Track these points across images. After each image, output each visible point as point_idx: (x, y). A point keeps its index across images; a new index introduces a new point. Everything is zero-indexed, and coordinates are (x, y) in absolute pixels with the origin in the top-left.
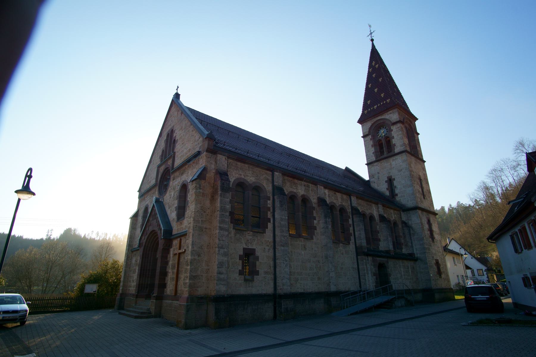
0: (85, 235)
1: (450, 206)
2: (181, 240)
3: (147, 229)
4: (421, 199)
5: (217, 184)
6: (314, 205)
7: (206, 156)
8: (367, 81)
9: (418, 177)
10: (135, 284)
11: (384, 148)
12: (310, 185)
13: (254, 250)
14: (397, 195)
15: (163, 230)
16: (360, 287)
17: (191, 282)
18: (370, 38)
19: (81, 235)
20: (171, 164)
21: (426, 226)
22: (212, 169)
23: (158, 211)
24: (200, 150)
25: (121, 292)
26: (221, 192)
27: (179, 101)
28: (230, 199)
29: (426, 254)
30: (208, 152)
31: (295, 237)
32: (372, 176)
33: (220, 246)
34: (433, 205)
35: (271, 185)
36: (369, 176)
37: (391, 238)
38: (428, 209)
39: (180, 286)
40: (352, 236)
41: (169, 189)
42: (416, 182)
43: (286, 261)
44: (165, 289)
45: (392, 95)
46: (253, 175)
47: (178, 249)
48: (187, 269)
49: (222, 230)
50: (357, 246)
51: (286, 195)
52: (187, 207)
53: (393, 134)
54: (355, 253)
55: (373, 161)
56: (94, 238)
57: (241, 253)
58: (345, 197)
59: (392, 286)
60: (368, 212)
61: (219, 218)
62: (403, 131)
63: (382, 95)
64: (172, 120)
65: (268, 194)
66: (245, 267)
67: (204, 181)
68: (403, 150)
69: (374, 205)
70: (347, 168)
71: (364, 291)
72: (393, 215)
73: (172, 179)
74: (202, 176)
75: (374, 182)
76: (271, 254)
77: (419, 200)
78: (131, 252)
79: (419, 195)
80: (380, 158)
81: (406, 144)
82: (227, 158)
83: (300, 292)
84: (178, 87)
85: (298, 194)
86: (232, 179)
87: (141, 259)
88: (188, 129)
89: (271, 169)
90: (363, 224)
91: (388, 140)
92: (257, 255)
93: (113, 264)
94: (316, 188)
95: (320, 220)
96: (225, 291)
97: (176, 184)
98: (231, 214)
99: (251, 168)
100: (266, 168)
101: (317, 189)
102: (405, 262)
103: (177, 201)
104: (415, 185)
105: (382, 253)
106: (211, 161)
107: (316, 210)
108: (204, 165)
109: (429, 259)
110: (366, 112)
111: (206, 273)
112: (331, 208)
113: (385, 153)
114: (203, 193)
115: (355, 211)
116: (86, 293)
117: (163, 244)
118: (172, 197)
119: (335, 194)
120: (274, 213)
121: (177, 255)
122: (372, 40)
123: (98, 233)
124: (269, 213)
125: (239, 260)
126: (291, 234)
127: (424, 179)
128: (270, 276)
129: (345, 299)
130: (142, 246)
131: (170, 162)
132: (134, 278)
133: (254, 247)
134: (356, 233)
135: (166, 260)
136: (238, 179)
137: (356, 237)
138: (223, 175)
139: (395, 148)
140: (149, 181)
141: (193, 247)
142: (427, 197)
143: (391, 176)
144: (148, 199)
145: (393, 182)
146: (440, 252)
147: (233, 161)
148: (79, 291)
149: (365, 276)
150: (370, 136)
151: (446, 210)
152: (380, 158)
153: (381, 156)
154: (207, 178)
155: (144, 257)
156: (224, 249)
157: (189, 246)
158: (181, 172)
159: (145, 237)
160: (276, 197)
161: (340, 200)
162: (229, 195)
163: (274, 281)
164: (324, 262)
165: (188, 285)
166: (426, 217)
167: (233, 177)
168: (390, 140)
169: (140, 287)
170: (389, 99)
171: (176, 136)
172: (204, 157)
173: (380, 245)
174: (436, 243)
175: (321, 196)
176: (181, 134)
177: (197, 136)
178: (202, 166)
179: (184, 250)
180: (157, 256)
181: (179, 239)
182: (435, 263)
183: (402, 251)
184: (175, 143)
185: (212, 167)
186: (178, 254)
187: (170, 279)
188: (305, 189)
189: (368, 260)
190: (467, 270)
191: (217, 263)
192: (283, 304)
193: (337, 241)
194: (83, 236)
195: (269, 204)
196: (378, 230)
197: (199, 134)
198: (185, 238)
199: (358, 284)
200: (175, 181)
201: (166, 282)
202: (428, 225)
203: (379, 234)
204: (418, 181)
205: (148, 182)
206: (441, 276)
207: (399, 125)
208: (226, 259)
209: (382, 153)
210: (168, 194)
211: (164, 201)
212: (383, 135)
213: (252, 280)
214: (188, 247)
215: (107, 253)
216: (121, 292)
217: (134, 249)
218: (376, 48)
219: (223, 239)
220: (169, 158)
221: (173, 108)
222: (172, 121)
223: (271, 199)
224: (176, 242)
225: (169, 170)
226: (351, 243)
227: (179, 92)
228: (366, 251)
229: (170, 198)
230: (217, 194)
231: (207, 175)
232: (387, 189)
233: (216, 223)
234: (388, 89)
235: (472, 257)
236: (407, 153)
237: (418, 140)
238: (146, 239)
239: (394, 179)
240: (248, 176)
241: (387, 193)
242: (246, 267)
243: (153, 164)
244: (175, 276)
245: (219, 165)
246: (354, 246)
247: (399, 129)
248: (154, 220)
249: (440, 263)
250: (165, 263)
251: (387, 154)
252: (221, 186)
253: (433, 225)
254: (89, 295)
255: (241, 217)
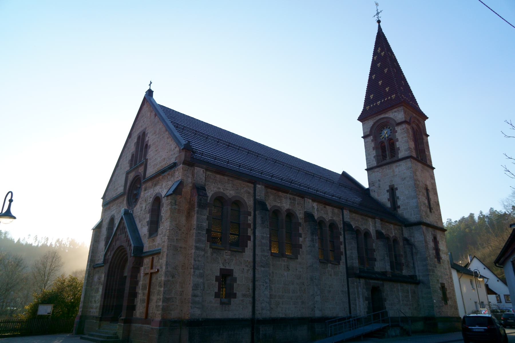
0: (19, 240)
1: (481, 213)
2: (153, 258)
3: (114, 244)
4: (426, 213)
5: (194, 200)
6: (300, 221)
7: (182, 169)
8: (371, 64)
9: (425, 187)
10: (98, 305)
11: (387, 152)
12: (297, 198)
13: (232, 271)
14: (399, 207)
15: (134, 246)
16: (465, 312)
17: (164, 304)
18: (376, 18)
19: (14, 239)
20: (143, 172)
21: (431, 245)
22: (189, 183)
23: (127, 225)
24: (176, 161)
25: (79, 313)
26: (198, 209)
27: (152, 100)
28: (207, 216)
29: (429, 276)
30: (185, 165)
31: (277, 257)
32: (372, 184)
33: (195, 266)
34: (442, 220)
35: (252, 199)
36: (369, 183)
37: (389, 258)
38: (435, 224)
39: (151, 308)
40: (343, 255)
41: (140, 200)
42: (421, 193)
43: (266, 283)
44: (134, 312)
45: (398, 90)
46: (233, 189)
47: (150, 269)
48: (160, 291)
49: (198, 250)
50: (348, 266)
51: (268, 211)
52: (161, 222)
53: (397, 136)
54: (345, 274)
55: (374, 166)
56: (31, 243)
57: (218, 274)
58: (336, 210)
59: (387, 312)
60: (363, 228)
61: (195, 236)
62: (409, 132)
63: (387, 89)
64: (144, 121)
65: (249, 209)
66: (221, 290)
67: (180, 196)
68: (408, 155)
69: (370, 220)
70: (344, 174)
71: (354, 317)
72: (392, 231)
73: (143, 189)
74: (178, 191)
75: (374, 191)
76: (250, 275)
77: (424, 214)
78: (93, 268)
79: (424, 208)
80: (382, 163)
81: (412, 148)
82: (205, 170)
83: (281, 317)
84: (151, 83)
85: (282, 208)
86: (210, 194)
87: (106, 278)
88: (162, 135)
89: (253, 180)
90: (356, 242)
91: (392, 142)
92: (235, 276)
93: (69, 281)
94: (303, 201)
95: (306, 238)
96: (199, 314)
97: (147, 196)
98: (208, 231)
99: (231, 181)
100: (248, 180)
101: (304, 202)
102: (405, 285)
103: (149, 214)
104: (420, 196)
105: (377, 275)
106: (187, 175)
107: (302, 226)
108: (180, 178)
109: (433, 282)
110: (368, 108)
111: (180, 296)
112: (321, 223)
113: (388, 158)
114: (179, 210)
115: (347, 226)
116: (39, 315)
117: (133, 263)
118: (143, 209)
119: (325, 207)
120: (255, 230)
121: (149, 275)
122: (379, 22)
123: (37, 238)
124: (249, 230)
125: (216, 281)
126: (274, 253)
127: (432, 189)
128: (249, 299)
129: (329, 326)
130: (107, 262)
131: (141, 170)
132: (97, 299)
133: (232, 268)
134: (348, 252)
135: (135, 280)
136: (215, 193)
137: (347, 256)
138: (200, 189)
139: (399, 152)
140: (116, 188)
141: (167, 268)
142: (434, 210)
143: (393, 185)
144: (114, 208)
145: (395, 192)
146: (447, 275)
147: (211, 173)
148: (31, 313)
149: (355, 300)
150: (372, 137)
151: (476, 218)
152: (382, 163)
153: (383, 160)
154: (183, 193)
155: (109, 275)
156: (200, 270)
157: (163, 266)
158: (154, 183)
159: (111, 252)
160: (257, 212)
161: (330, 214)
162: (206, 212)
163: (252, 305)
164: (309, 285)
165: (161, 307)
166: (432, 234)
167: (211, 191)
168: (394, 143)
169: (105, 308)
170: (395, 95)
171: (148, 140)
172: (180, 170)
173: (376, 266)
174: (442, 264)
175: (308, 210)
176: (154, 139)
177: (173, 145)
178: (178, 179)
179: (156, 270)
180: (126, 274)
181: (151, 258)
182: (440, 288)
183: (402, 272)
184: (147, 148)
185: (189, 180)
186: (149, 273)
187: (141, 301)
188: (291, 203)
189: (359, 282)
190: (489, 296)
191: (192, 285)
192: (261, 330)
193: (324, 261)
194: (16, 241)
195: (249, 220)
196: (374, 248)
197: (175, 142)
198: (158, 256)
199: (347, 310)
200: (146, 191)
201: (135, 304)
202: (433, 243)
203: (375, 253)
204: (425, 191)
205: (115, 188)
206: (447, 302)
207: (404, 126)
208: (201, 280)
209: (384, 157)
210: (138, 206)
211: (134, 213)
212: (387, 136)
213: (229, 303)
214: (161, 268)
215: (53, 264)
216: (79, 313)
217: (96, 264)
218: (382, 32)
219: (199, 260)
220: (141, 165)
221: (145, 106)
222: (143, 122)
223: (252, 214)
224: (147, 261)
225: (140, 178)
226: (341, 263)
227: (152, 89)
228: (358, 272)
229: (141, 210)
230: (194, 211)
231: (183, 190)
232: (389, 200)
233: (192, 242)
234: (394, 82)
235: (498, 279)
236: (412, 159)
237: (427, 142)
238: (112, 255)
239: (397, 189)
240: (227, 190)
241: (389, 205)
242: (223, 290)
243: (121, 168)
244: (146, 298)
245: (196, 178)
246: (345, 266)
247: (404, 131)
248: (122, 234)
249: (446, 287)
250: (135, 283)
251: (390, 159)
252: (198, 202)
253: (440, 243)
254: (42, 317)
255: (219, 234)
